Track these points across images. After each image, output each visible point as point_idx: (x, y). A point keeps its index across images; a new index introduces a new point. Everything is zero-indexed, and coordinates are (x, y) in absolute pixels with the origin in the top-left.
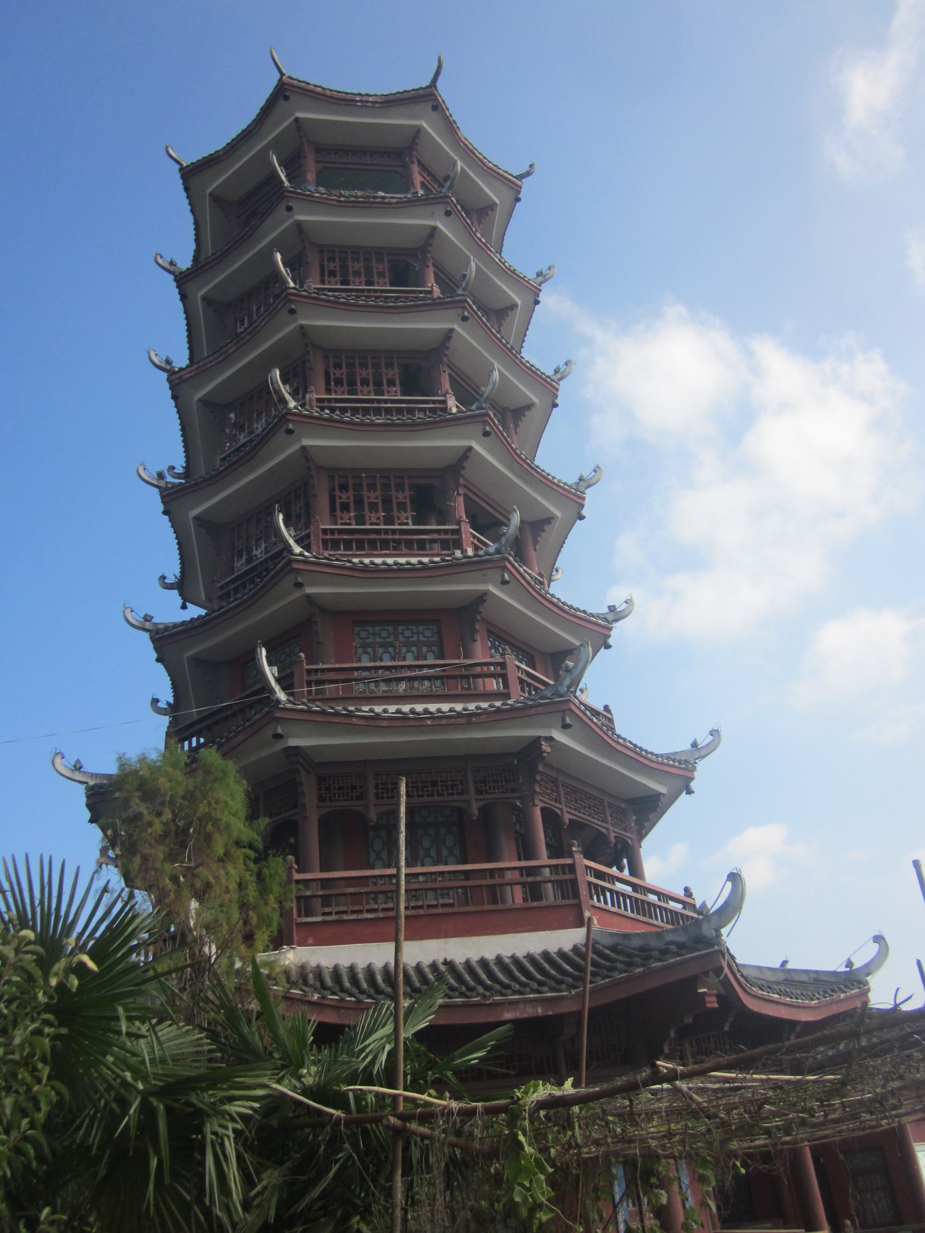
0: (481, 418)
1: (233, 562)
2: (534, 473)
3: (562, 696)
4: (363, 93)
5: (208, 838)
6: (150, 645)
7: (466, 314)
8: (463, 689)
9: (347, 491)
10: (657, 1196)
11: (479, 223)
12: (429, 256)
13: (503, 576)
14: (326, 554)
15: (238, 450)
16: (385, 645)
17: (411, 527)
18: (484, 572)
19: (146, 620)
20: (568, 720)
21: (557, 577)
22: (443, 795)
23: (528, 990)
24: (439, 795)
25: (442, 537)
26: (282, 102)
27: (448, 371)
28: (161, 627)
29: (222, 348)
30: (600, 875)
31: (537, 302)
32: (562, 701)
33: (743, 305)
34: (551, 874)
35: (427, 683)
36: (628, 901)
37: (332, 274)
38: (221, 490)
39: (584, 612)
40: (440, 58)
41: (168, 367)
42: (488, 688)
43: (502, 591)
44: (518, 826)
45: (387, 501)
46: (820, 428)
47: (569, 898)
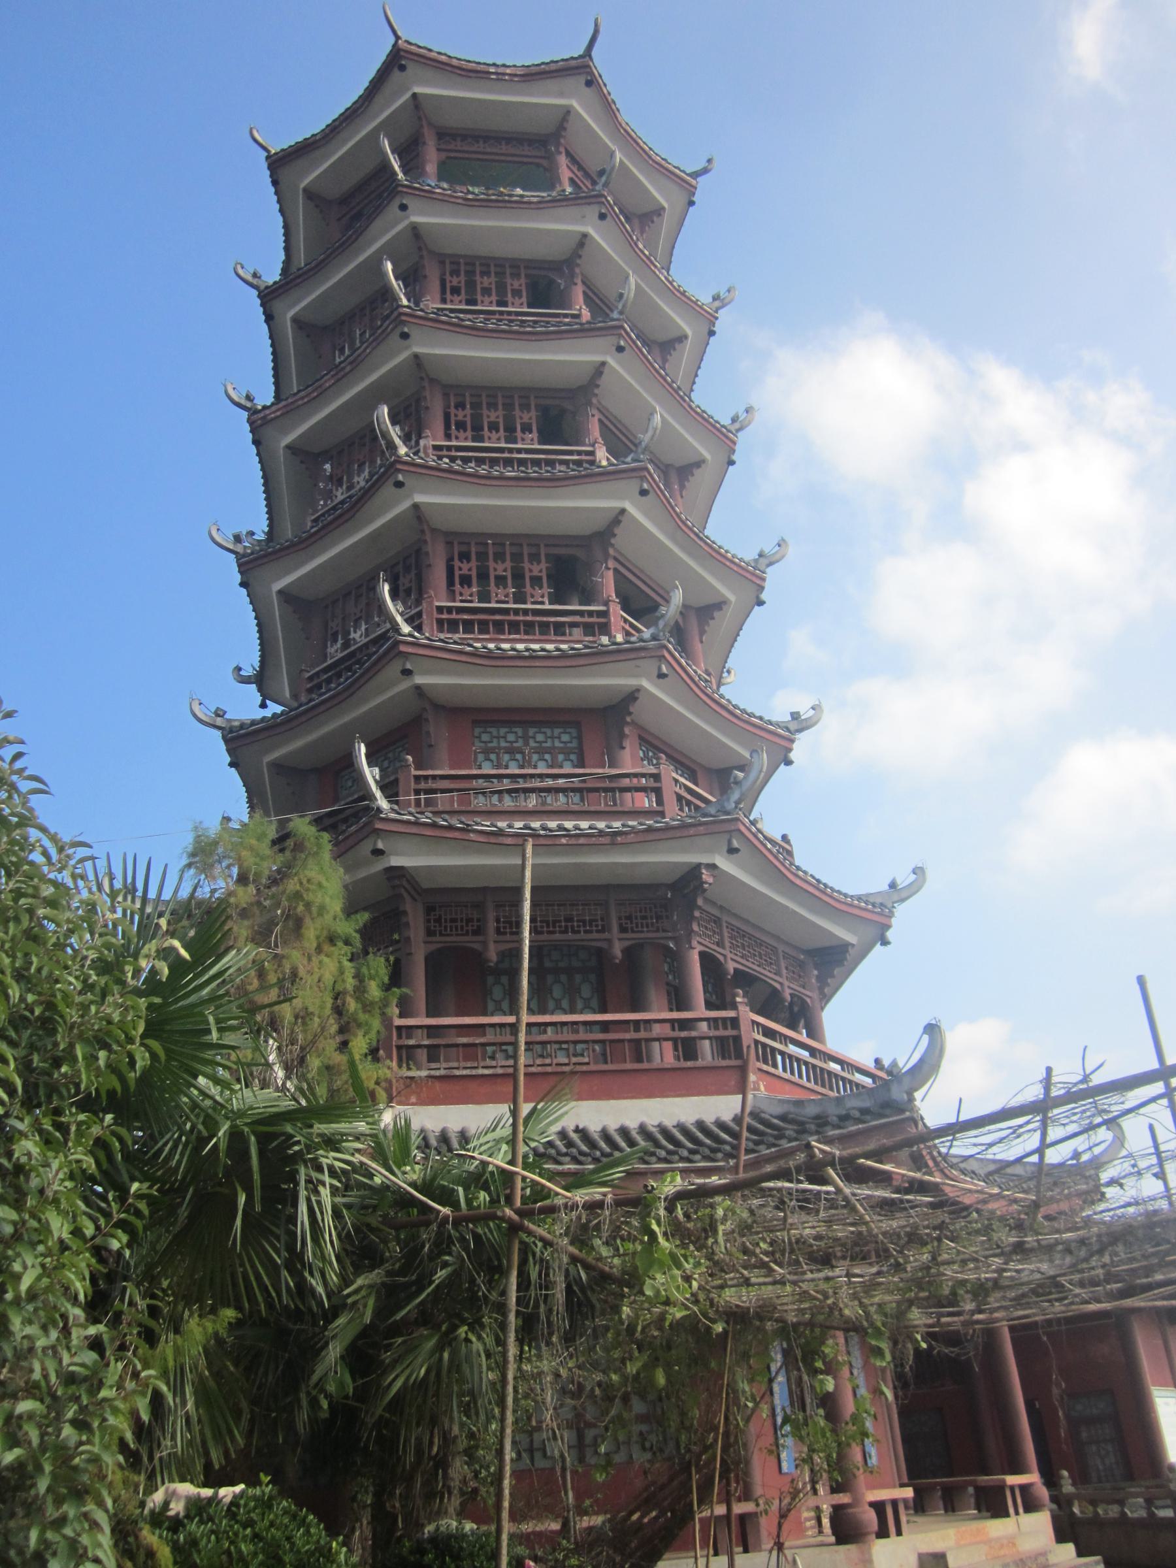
0: (638, 472)
1: (326, 647)
2: (702, 544)
3: (728, 813)
4: (499, 63)
5: (299, 923)
6: (222, 746)
7: (622, 343)
8: (606, 804)
9: (469, 561)
10: (822, 1382)
11: (642, 232)
12: (577, 270)
13: (660, 668)
14: (442, 636)
15: (334, 508)
16: (511, 751)
17: (547, 607)
18: (638, 662)
19: (218, 715)
20: (735, 844)
21: (729, 680)
22: (579, 932)
23: (676, 1157)
24: (574, 932)
25: (586, 619)
26: (396, 74)
27: (598, 416)
28: (237, 724)
29: (317, 380)
30: (769, 1033)
31: (712, 333)
32: (728, 820)
33: (957, 316)
34: (709, 1028)
35: (562, 798)
36: (804, 1068)
37: (456, 291)
38: (313, 557)
39: (761, 718)
40: (596, 20)
41: (249, 405)
42: (638, 805)
43: (657, 686)
44: (670, 977)
45: (518, 576)
46: (1058, 487)
47: (730, 1058)
